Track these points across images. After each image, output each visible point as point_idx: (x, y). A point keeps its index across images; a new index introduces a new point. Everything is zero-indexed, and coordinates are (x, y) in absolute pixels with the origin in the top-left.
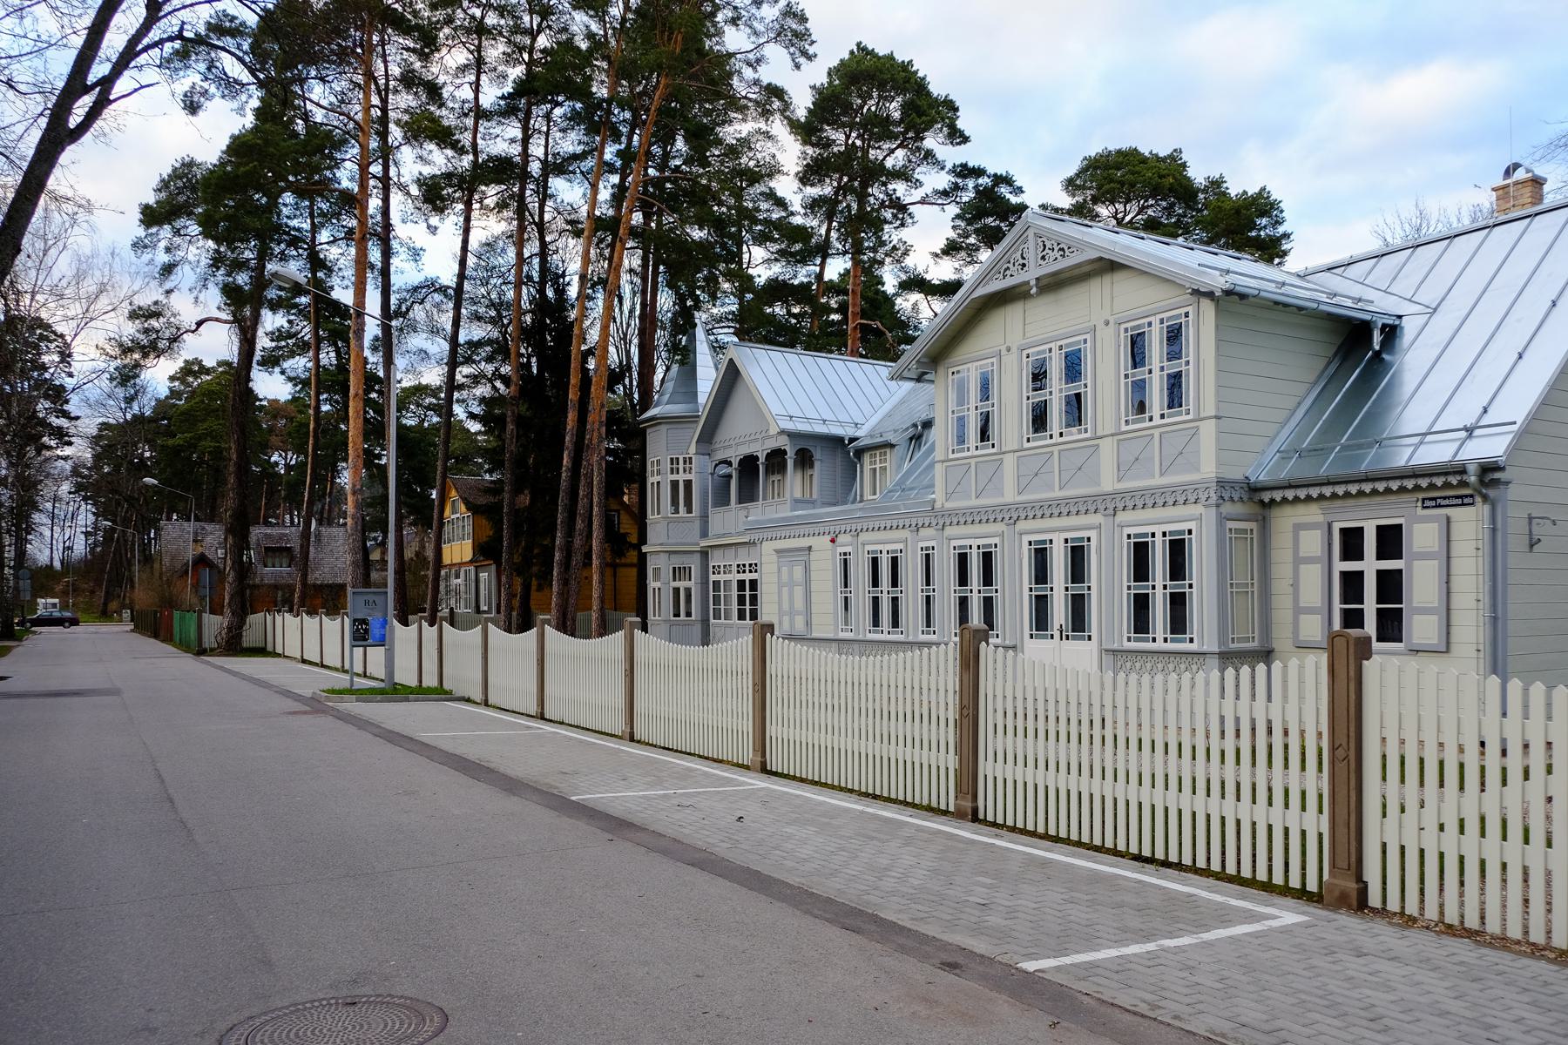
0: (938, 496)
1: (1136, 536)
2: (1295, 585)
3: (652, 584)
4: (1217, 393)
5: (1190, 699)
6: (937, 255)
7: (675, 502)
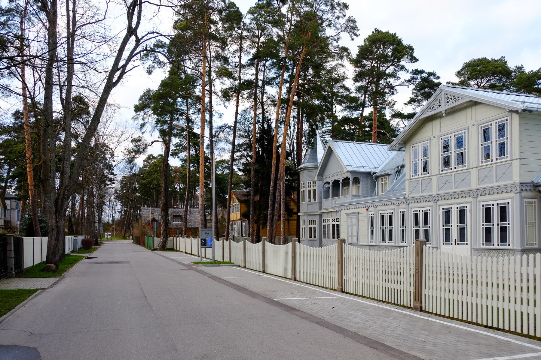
1: (486, 205)
3: (302, 226)
6: (406, 104)
7: (310, 197)
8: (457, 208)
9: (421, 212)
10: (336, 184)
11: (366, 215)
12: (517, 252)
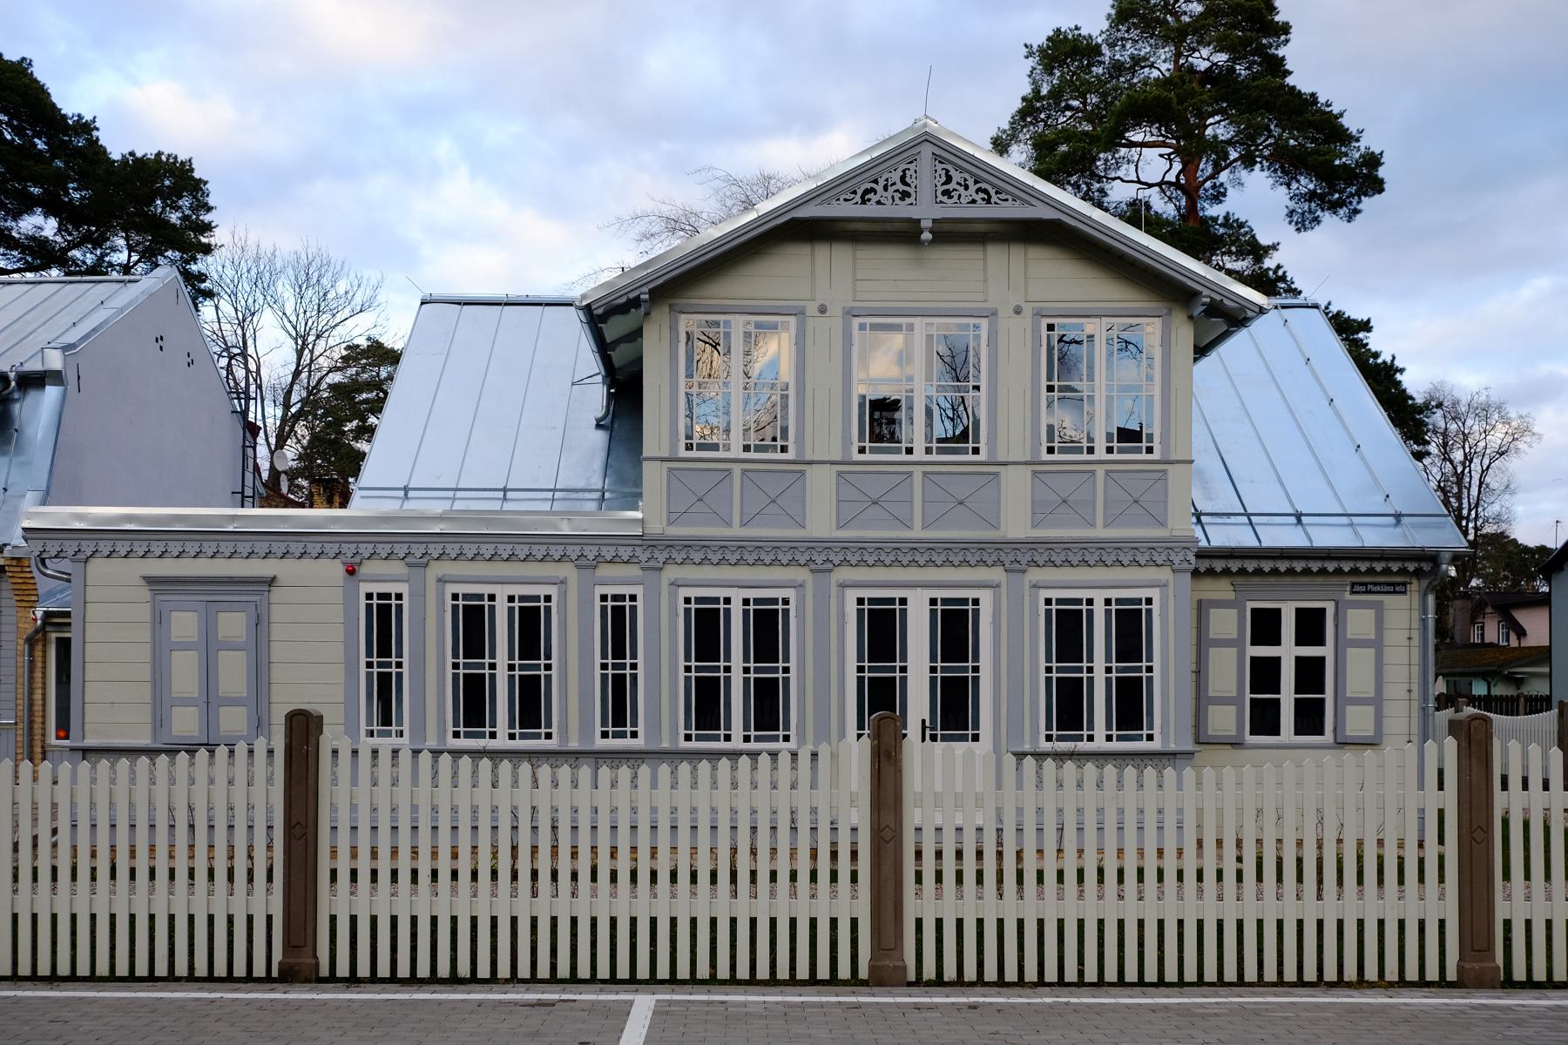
8: (933, 602)
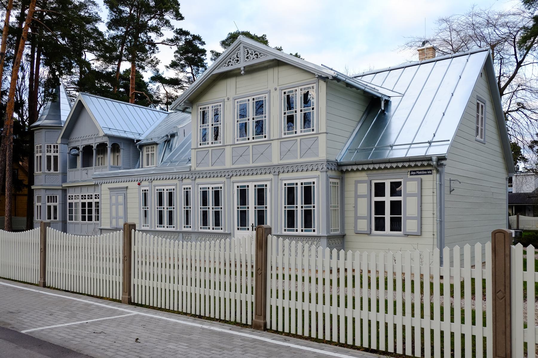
0: (193, 164)
1: (288, 184)
2: (356, 207)
3: (36, 204)
4: (327, 123)
5: (206, 251)
6: (167, 67)
8: (255, 186)
9: (211, 190)
10: (88, 150)
11: (136, 191)
12: (322, 240)
